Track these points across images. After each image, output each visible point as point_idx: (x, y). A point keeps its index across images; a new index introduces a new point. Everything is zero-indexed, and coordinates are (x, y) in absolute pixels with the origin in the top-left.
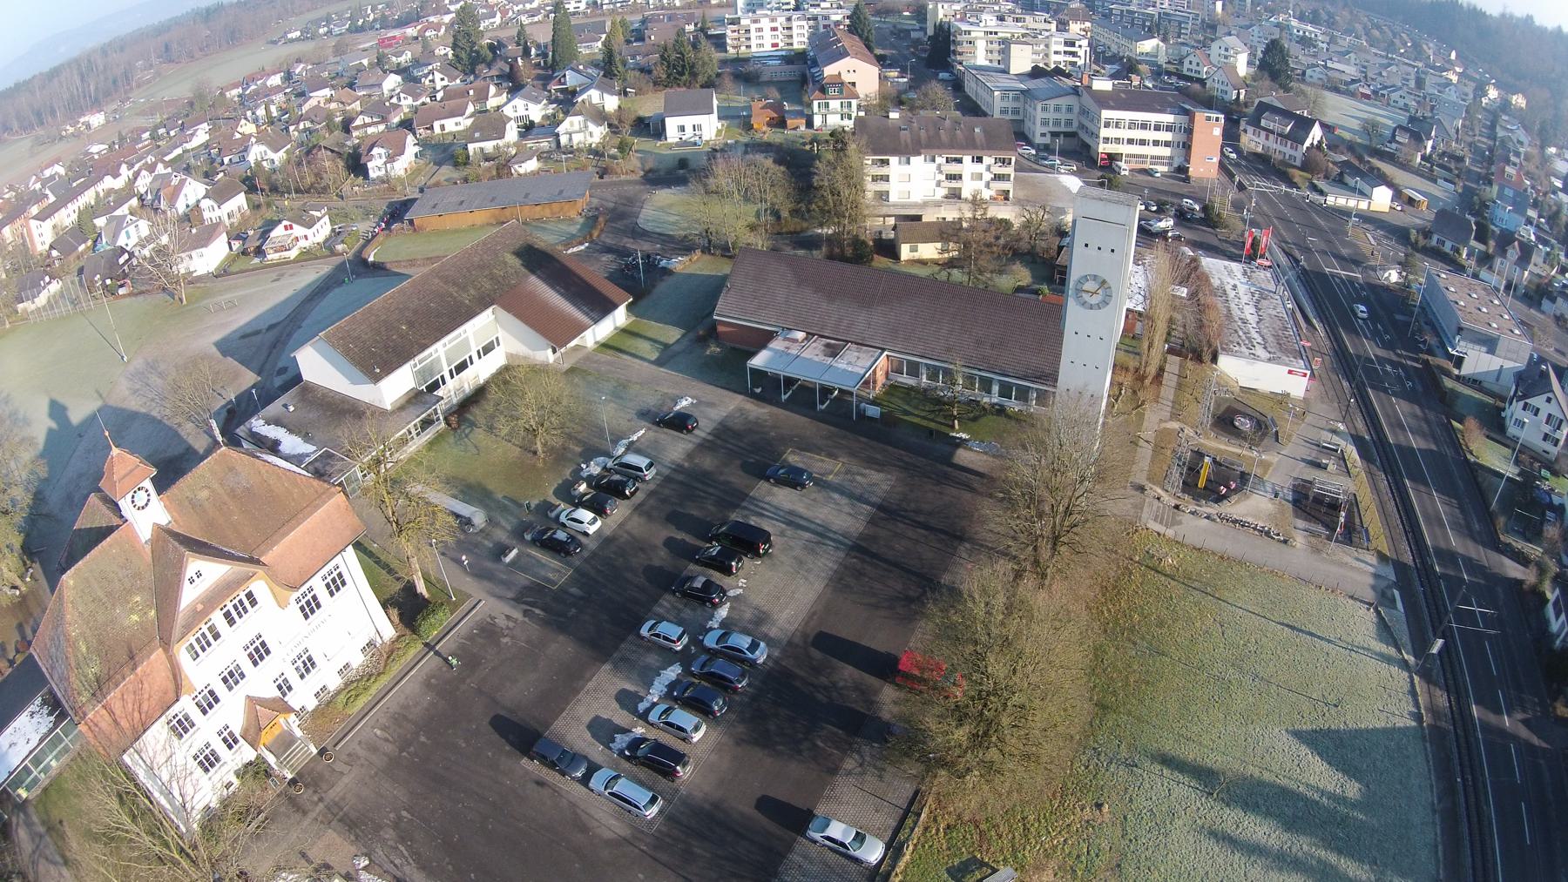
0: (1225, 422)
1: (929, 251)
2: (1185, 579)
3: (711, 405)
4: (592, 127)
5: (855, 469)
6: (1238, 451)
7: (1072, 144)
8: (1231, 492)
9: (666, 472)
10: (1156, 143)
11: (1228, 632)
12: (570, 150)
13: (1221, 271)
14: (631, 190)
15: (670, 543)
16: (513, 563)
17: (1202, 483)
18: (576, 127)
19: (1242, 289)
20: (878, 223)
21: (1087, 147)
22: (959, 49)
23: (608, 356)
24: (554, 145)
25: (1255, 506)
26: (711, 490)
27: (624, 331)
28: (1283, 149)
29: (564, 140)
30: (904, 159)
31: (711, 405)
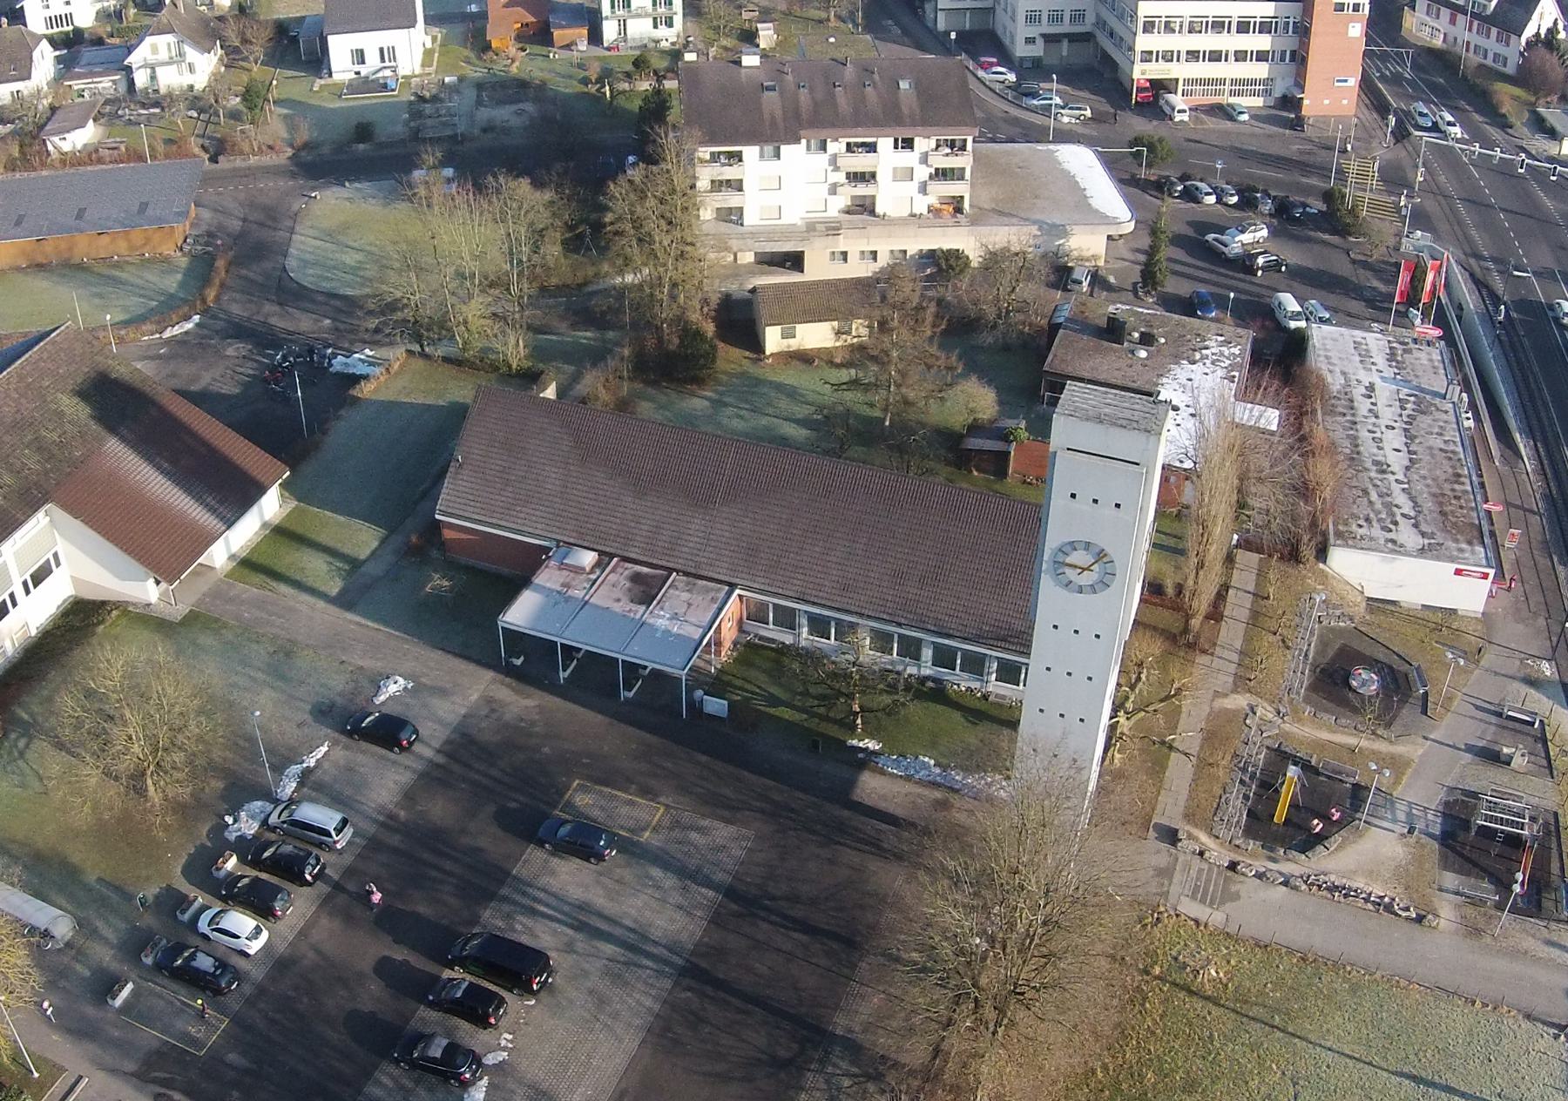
0: (1331, 682)
1: (816, 335)
2: (1236, 1003)
3: (443, 692)
4: (192, 54)
6: (1351, 741)
7: (1082, 55)
8: (1333, 827)
9: (371, 829)
10: (1241, 56)
12: (157, 101)
13: (1342, 350)
15: (384, 968)
16: (127, 1008)
17: (1280, 814)
18: (163, 55)
19: (1385, 392)
20: (728, 263)
23: (251, 589)
24: (122, 88)
25: (1372, 853)
26: (448, 865)
27: (280, 533)
29: (141, 79)
30: (769, 149)
31: (442, 692)
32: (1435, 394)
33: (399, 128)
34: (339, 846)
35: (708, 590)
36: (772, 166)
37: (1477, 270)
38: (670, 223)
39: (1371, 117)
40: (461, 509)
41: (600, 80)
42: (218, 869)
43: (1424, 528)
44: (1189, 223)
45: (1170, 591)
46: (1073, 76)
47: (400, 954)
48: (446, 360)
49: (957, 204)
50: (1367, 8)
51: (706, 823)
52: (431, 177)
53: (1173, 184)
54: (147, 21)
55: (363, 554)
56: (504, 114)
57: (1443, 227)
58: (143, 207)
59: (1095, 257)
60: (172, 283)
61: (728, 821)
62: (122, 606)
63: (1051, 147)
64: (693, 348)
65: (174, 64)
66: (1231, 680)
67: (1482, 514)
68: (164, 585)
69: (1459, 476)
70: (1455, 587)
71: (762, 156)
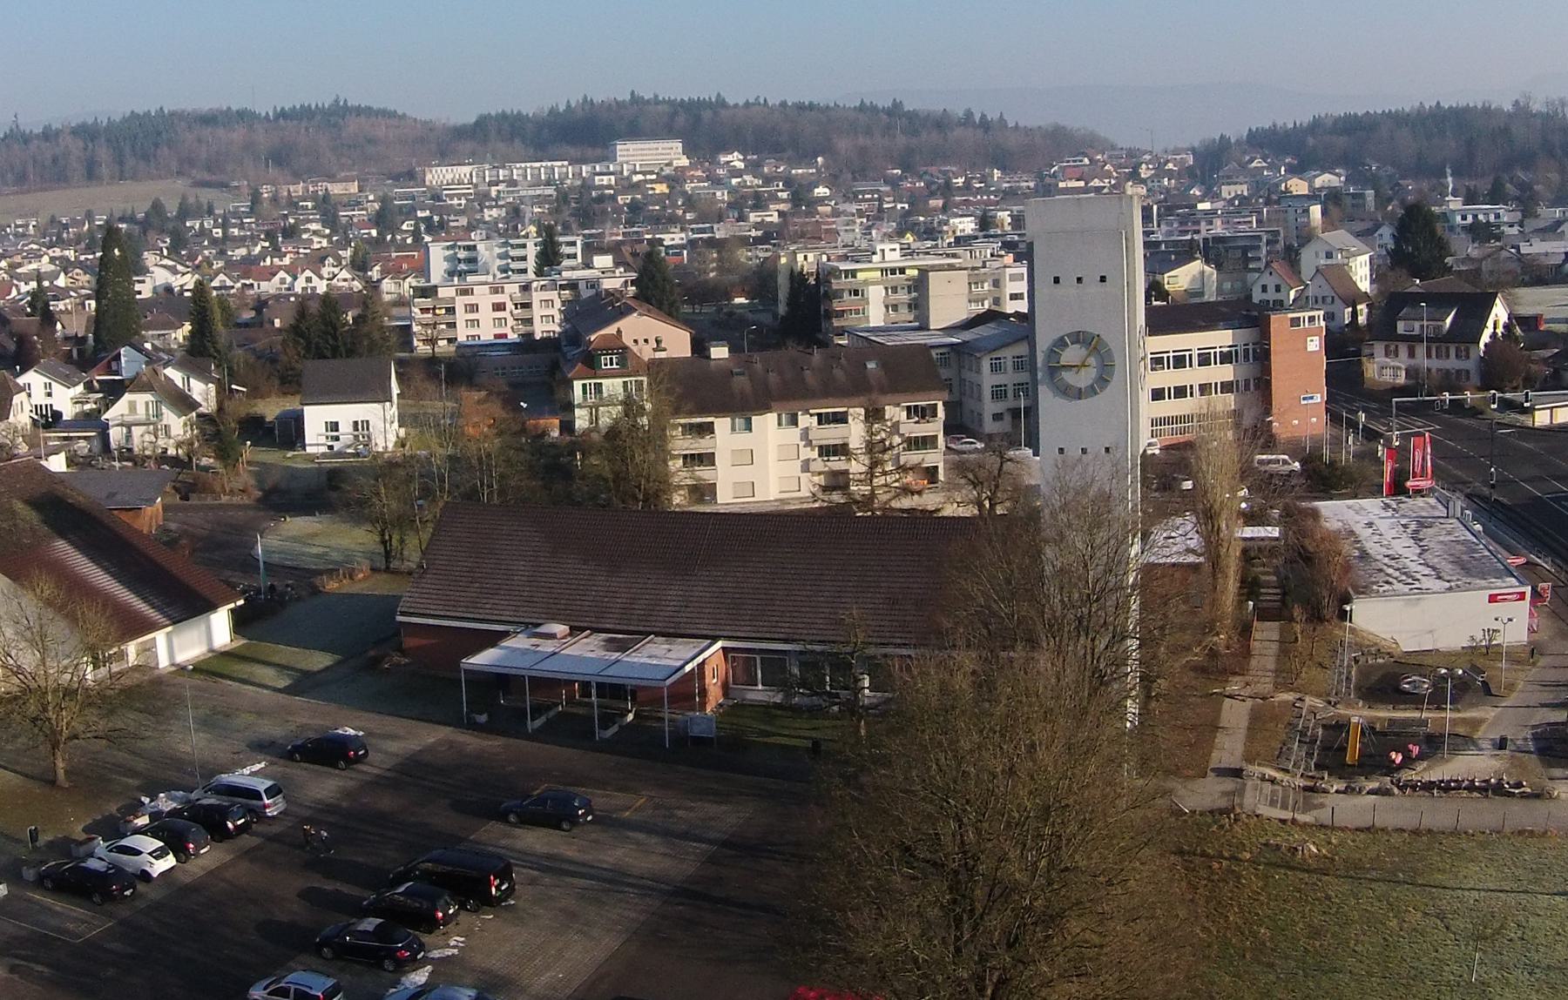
6: (1417, 715)
12: (127, 454)
22: (837, 306)
29: (116, 435)
36: (743, 440)
71: (733, 429)
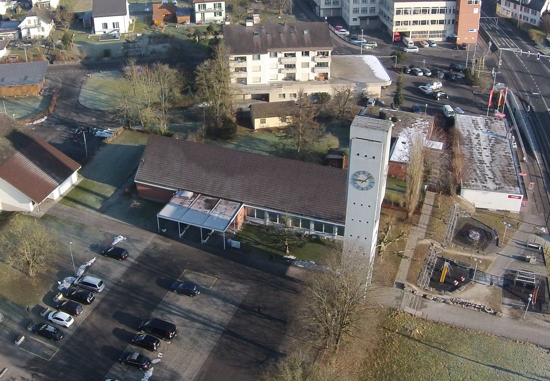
0: (462, 235)
1: (273, 122)
3: (138, 241)
4: (43, 24)
5: (227, 282)
8: (461, 283)
10: (433, 22)
11: (453, 373)
12: (30, 41)
14: (72, 73)
15: (116, 332)
16: (21, 345)
17: (442, 279)
18: (33, 24)
19: (483, 137)
20: (242, 99)
21: (385, 27)
23: (66, 207)
24: (17, 36)
25: (477, 292)
27: (78, 188)
28: (526, 14)
29: (24, 33)
30: (256, 56)
32: (503, 137)
33: (120, 52)
34: (99, 291)
35: (233, 204)
36: (257, 62)
37: (521, 95)
38: (219, 81)
39: (482, 43)
40: (143, 179)
41: (194, 35)
42: (56, 299)
43: (497, 182)
44: (413, 83)
45: (402, 205)
46: (369, 32)
47: (122, 327)
48: (138, 131)
49: (325, 76)
50: (481, 2)
51: (233, 283)
52: (133, 69)
53: (407, 69)
54: (26, 13)
55: (109, 195)
56: (159, 47)
57: (509, 81)
58: (26, 78)
59: (377, 95)
60: (37, 105)
61: (241, 283)
62: (20, 213)
63: (361, 56)
64: (227, 128)
65: (37, 28)
66: (424, 234)
67: (519, 177)
68: (36, 204)
69: (510, 164)
70: (509, 202)
71: (253, 59)
